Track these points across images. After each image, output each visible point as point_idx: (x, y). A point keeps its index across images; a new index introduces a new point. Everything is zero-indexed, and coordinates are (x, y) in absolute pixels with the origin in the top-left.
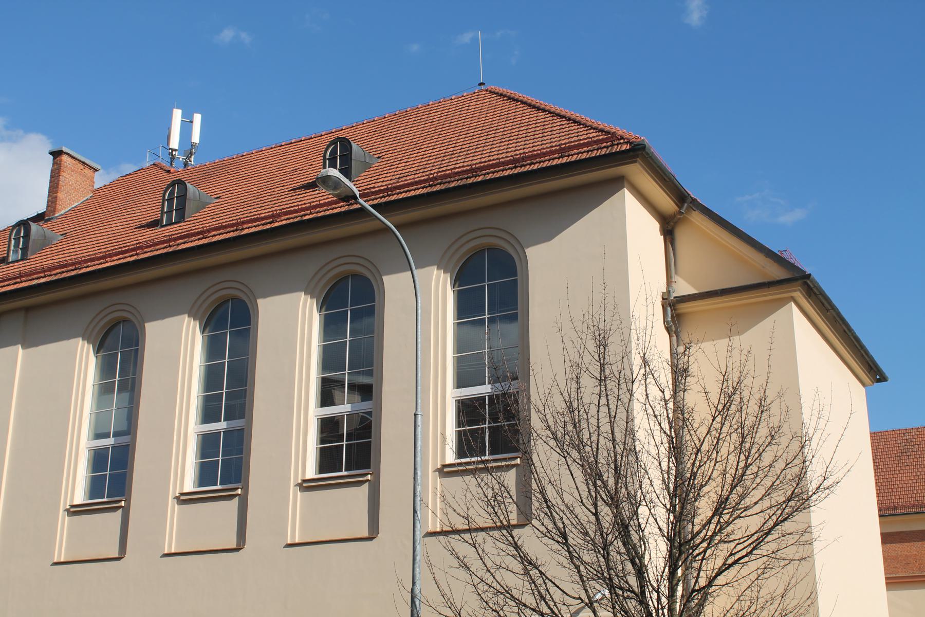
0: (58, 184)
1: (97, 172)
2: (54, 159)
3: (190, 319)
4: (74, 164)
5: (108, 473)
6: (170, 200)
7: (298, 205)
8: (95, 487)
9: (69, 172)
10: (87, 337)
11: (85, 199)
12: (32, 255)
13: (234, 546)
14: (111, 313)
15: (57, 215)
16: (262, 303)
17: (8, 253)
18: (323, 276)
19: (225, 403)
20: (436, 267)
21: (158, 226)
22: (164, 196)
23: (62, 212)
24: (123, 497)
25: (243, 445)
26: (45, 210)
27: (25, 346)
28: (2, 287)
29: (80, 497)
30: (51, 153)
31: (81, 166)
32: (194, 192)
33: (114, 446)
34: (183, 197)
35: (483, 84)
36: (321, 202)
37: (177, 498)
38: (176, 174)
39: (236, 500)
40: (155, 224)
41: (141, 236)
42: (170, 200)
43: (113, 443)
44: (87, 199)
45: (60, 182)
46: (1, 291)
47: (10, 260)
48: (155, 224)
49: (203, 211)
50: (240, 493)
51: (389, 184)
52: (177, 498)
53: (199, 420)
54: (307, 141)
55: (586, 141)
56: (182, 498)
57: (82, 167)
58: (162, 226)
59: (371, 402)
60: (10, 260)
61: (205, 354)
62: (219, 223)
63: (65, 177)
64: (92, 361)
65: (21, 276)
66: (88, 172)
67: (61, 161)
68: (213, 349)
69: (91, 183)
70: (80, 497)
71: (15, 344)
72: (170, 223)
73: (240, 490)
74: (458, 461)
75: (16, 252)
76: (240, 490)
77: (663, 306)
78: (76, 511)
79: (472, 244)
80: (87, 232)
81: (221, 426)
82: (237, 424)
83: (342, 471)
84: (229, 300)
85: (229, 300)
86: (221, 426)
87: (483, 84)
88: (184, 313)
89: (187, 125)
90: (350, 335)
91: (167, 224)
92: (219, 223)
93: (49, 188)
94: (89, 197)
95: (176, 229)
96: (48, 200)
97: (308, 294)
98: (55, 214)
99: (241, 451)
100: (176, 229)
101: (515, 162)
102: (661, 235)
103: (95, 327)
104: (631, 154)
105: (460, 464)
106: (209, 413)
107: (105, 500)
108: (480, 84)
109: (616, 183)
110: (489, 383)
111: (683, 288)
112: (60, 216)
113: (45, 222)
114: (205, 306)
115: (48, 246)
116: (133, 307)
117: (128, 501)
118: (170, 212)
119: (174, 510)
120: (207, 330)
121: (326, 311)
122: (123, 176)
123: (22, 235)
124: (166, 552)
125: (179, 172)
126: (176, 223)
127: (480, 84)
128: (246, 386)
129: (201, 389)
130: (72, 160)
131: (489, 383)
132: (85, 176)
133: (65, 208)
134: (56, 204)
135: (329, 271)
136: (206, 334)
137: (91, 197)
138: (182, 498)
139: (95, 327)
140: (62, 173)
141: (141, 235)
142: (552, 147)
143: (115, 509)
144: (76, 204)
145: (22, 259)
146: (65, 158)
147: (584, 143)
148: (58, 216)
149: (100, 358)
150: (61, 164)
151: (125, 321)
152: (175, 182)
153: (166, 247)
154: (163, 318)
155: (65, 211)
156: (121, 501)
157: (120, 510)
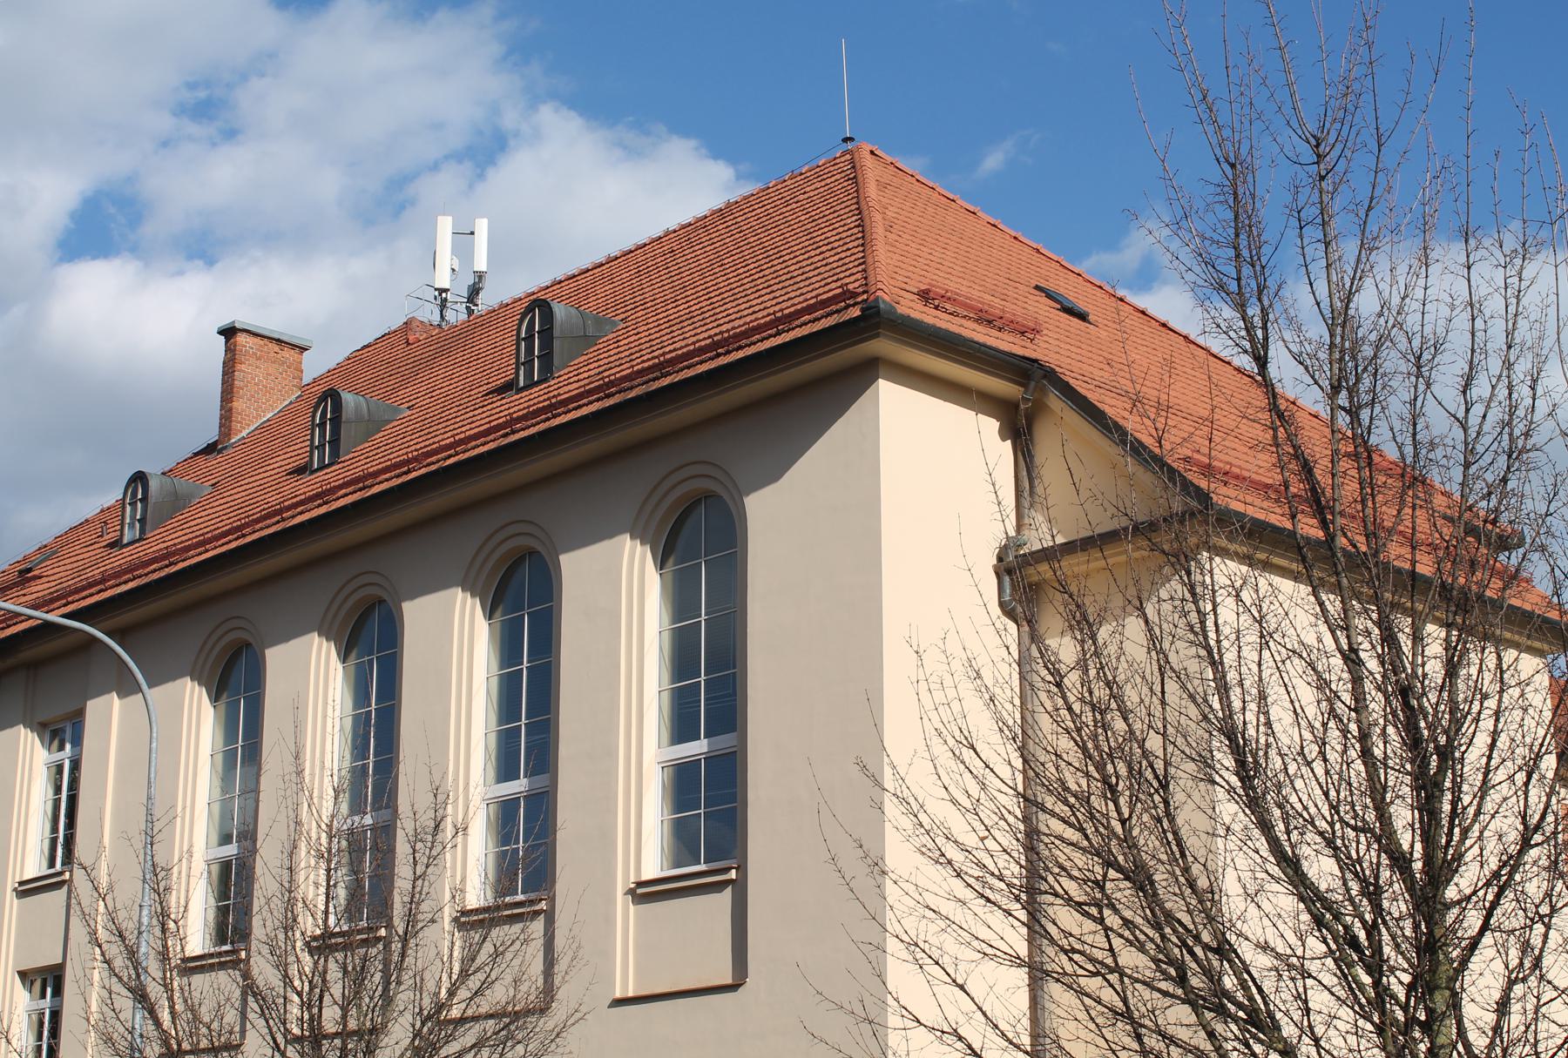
0: (232, 385)
1: (306, 353)
2: (226, 342)
3: (465, 594)
4: (261, 346)
5: (702, 811)
7: (305, 493)
8: (683, 840)
9: (252, 361)
10: (469, 586)
11: (287, 403)
12: (152, 531)
14: (355, 590)
15: (233, 441)
16: (407, 607)
19: (526, 743)
20: (628, 536)
21: (305, 473)
23: (244, 434)
24: (734, 860)
25: (736, 787)
26: (217, 438)
27: (122, 695)
28: (3, 629)
29: (653, 866)
30: (221, 332)
31: (275, 347)
32: (357, 407)
33: (708, 755)
34: (547, 333)
36: (697, 345)
37: (631, 892)
38: (799, 179)
39: (728, 891)
40: (508, 387)
41: (836, 281)
42: (530, 338)
43: (236, 852)
44: (291, 403)
45: (236, 382)
46: (3, 636)
47: (125, 541)
48: (508, 387)
49: (576, 362)
50: (734, 877)
51: (716, 335)
52: (631, 892)
53: (492, 774)
54: (583, 276)
55: (743, 328)
57: (277, 348)
58: (520, 390)
59: (735, 734)
60: (125, 541)
61: (352, 694)
62: (769, 315)
63: (244, 372)
65: (103, 580)
66: (288, 354)
67: (235, 346)
68: (681, 602)
69: (297, 373)
71: (109, 692)
72: (530, 385)
73: (734, 871)
74: (212, 950)
76: (734, 871)
77: (997, 574)
78: (646, 893)
79: (223, 643)
80: (717, 293)
81: (519, 786)
82: (726, 741)
83: (517, 894)
84: (700, 499)
85: (700, 499)
86: (519, 786)
87: (851, 139)
88: (182, 675)
89: (465, 235)
90: (529, 656)
91: (528, 383)
92: (769, 315)
93: (222, 393)
94: (293, 397)
95: (333, 476)
96: (221, 415)
97: (636, 538)
98: (230, 439)
99: (733, 798)
100: (333, 476)
102: (1004, 439)
103: (335, 616)
104: (862, 324)
105: (220, 954)
107: (702, 867)
108: (846, 140)
109: (863, 374)
110: (525, 777)
111: (1040, 537)
112: (239, 440)
113: (218, 454)
114: (489, 565)
115: (184, 509)
116: (540, 527)
117: (742, 868)
119: (625, 913)
121: (228, 698)
122: (358, 351)
123: (140, 496)
124: (618, 995)
125: (818, 167)
127: (846, 140)
128: (734, 668)
130: (257, 340)
131: (525, 777)
132: (284, 363)
133: (249, 425)
134: (231, 422)
135: (493, 551)
137: (297, 398)
139: (208, 655)
140: (238, 367)
141: (835, 278)
142: (633, 367)
143: (718, 887)
145: (140, 539)
146: (241, 339)
147: (802, 308)
148: (235, 442)
149: (669, 577)
150: (235, 350)
152: (328, 393)
153: (278, 522)
155: (248, 431)
156: (730, 869)
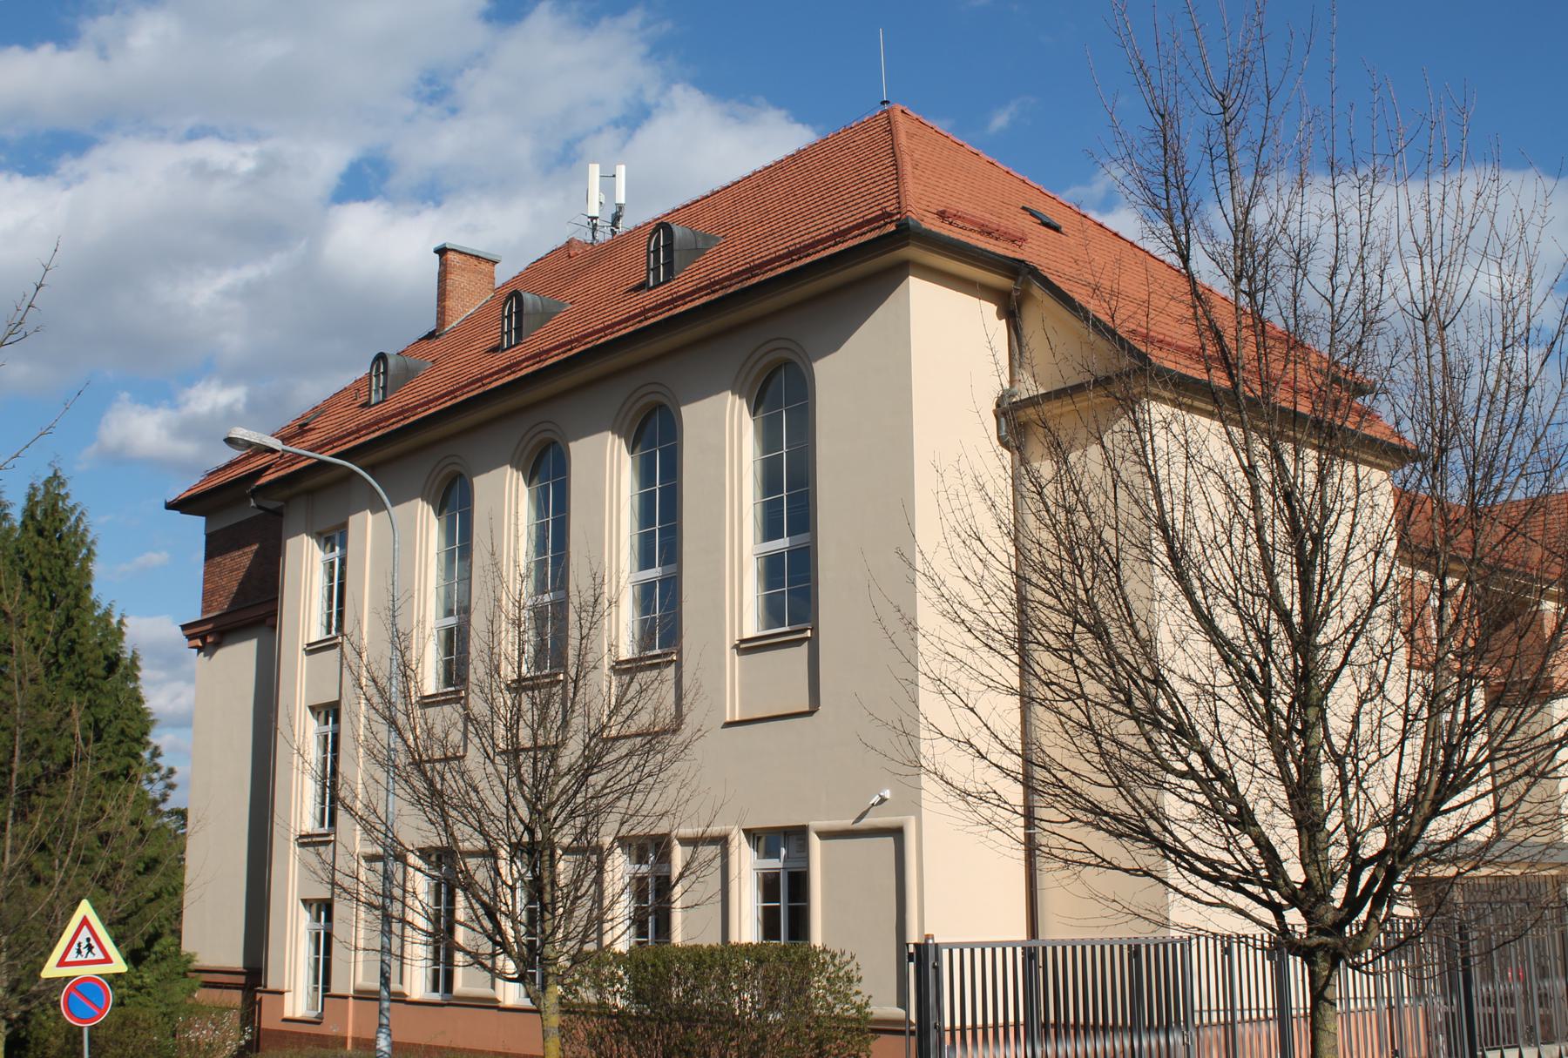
0: (445, 290)
6: (657, 251)
10: (617, 431)
13: (807, 708)
17: (370, 395)
18: (752, 367)
22: (649, 245)
23: (454, 324)
29: (751, 627)
32: (534, 304)
35: (887, 102)
37: (736, 647)
40: (642, 286)
47: (373, 402)
48: (642, 286)
52: (736, 647)
56: (743, 646)
58: (650, 289)
60: (373, 402)
64: (524, 491)
66: (484, 266)
68: (769, 439)
70: (751, 627)
75: (377, 391)
79: (766, 360)
81: (782, 544)
82: (802, 539)
86: (782, 544)
87: (887, 102)
89: (608, 178)
101: (790, 255)
106: (770, 529)
108: (883, 103)
109: (895, 275)
111: (1028, 388)
114: (632, 413)
118: (657, 269)
119: (733, 663)
120: (638, 449)
124: (728, 719)
126: (664, 283)
127: (883, 103)
129: (636, 525)
130: (462, 257)
136: (760, 415)
138: (743, 646)
140: (449, 276)
144: (472, 311)
145: (383, 401)
146: (450, 255)
149: (760, 421)
151: (787, 363)
154: (488, 470)
156: (806, 629)
157: (673, 665)
